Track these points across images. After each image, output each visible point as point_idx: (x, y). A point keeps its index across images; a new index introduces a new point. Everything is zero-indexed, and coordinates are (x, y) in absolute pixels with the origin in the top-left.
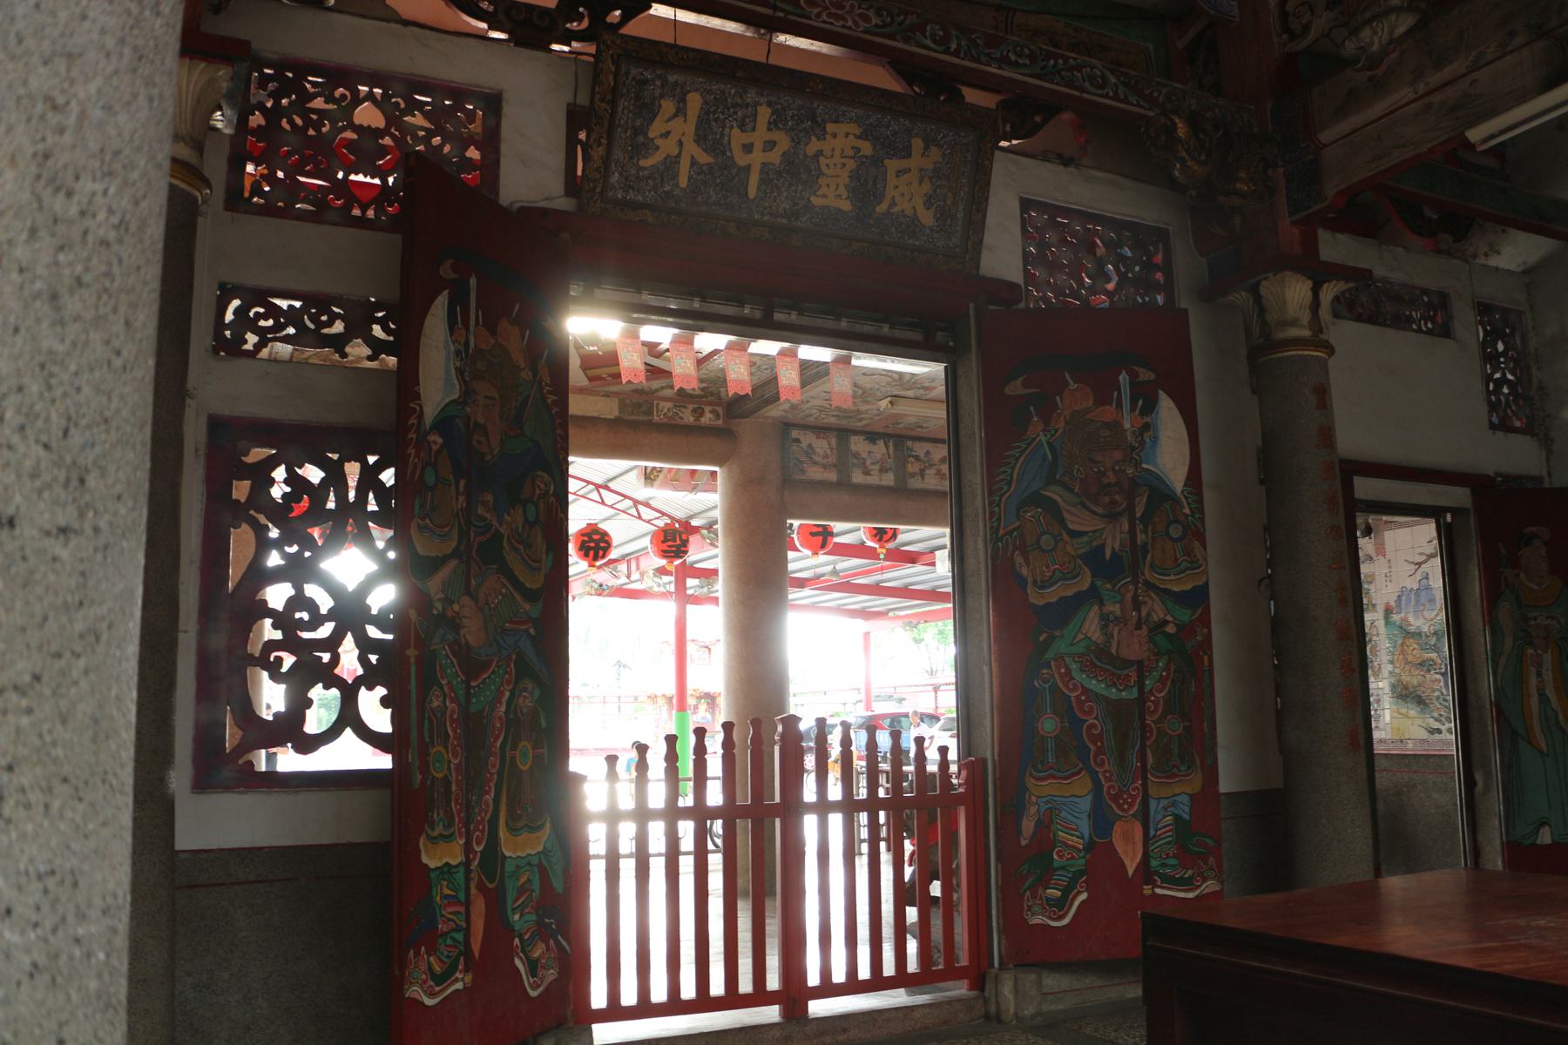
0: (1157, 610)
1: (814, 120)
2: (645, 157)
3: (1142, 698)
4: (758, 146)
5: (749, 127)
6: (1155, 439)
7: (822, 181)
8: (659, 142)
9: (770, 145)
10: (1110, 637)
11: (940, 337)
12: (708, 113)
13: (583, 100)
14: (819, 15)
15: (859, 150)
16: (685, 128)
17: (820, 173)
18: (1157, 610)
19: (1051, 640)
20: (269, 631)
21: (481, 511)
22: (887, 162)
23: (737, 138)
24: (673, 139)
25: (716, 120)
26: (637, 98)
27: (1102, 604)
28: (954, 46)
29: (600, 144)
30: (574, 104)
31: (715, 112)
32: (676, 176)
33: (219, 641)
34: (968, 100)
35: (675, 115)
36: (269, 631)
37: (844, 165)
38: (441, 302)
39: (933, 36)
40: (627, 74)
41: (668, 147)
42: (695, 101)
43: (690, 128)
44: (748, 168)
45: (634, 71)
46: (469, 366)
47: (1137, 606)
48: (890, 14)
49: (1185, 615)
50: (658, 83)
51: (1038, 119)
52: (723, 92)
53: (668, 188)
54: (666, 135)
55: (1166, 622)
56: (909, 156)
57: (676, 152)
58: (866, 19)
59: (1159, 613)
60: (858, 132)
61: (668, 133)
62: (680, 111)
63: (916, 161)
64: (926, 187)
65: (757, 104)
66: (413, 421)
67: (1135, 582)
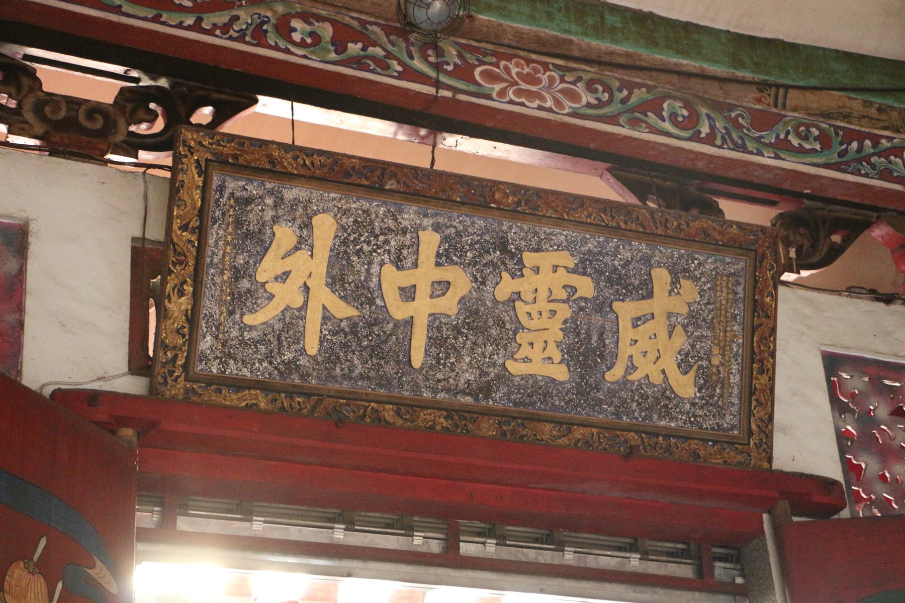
1: (504, 249)
2: (252, 311)
4: (423, 290)
5: (409, 262)
7: (522, 337)
8: (272, 287)
9: (442, 287)
11: (721, 571)
12: (345, 242)
13: (156, 233)
14: (502, 93)
15: (574, 290)
16: (313, 266)
17: (519, 327)
22: (616, 305)
23: (391, 279)
24: (295, 282)
25: (359, 253)
26: (238, 223)
28: (705, 130)
29: (181, 293)
30: (143, 239)
31: (356, 242)
32: (299, 337)
34: (728, 216)
35: (297, 248)
37: (553, 312)
39: (673, 117)
40: (221, 189)
41: (287, 296)
42: (325, 227)
45: (232, 185)
48: (608, 89)
50: (269, 201)
51: (836, 238)
52: (366, 212)
53: (288, 356)
56: (650, 295)
57: (299, 302)
58: (573, 96)
60: (571, 263)
61: (287, 274)
62: (303, 243)
63: (662, 301)
64: (680, 340)
65: (417, 228)
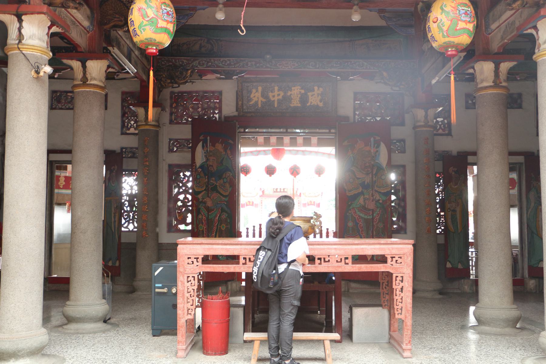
0: (377, 197)
3: (373, 219)
6: (379, 154)
10: (365, 203)
18: (377, 197)
19: (352, 203)
20: (180, 204)
21: (211, 181)
23: (270, 94)
27: (364, 195)
28: (317, 66)
32: (258, 105)
33: (171, 205)
36: (180, 204)
38: (200, 144)
43: (260, 94)
44: (274, 101)
46: (207, 156)
47: (373, 196)
49: (384, 198)
54: (255, 97)
55: (379, 200)
59: (378, 198)
66: (194, 167)
67: (372, 190)
